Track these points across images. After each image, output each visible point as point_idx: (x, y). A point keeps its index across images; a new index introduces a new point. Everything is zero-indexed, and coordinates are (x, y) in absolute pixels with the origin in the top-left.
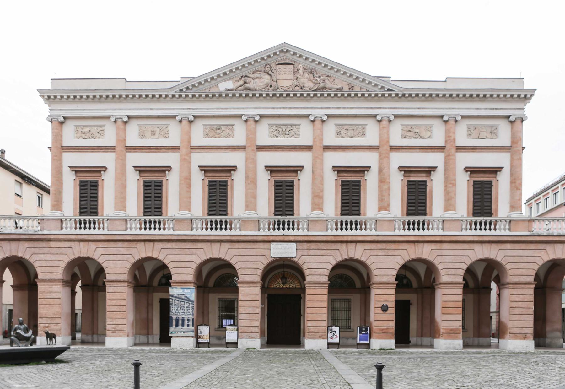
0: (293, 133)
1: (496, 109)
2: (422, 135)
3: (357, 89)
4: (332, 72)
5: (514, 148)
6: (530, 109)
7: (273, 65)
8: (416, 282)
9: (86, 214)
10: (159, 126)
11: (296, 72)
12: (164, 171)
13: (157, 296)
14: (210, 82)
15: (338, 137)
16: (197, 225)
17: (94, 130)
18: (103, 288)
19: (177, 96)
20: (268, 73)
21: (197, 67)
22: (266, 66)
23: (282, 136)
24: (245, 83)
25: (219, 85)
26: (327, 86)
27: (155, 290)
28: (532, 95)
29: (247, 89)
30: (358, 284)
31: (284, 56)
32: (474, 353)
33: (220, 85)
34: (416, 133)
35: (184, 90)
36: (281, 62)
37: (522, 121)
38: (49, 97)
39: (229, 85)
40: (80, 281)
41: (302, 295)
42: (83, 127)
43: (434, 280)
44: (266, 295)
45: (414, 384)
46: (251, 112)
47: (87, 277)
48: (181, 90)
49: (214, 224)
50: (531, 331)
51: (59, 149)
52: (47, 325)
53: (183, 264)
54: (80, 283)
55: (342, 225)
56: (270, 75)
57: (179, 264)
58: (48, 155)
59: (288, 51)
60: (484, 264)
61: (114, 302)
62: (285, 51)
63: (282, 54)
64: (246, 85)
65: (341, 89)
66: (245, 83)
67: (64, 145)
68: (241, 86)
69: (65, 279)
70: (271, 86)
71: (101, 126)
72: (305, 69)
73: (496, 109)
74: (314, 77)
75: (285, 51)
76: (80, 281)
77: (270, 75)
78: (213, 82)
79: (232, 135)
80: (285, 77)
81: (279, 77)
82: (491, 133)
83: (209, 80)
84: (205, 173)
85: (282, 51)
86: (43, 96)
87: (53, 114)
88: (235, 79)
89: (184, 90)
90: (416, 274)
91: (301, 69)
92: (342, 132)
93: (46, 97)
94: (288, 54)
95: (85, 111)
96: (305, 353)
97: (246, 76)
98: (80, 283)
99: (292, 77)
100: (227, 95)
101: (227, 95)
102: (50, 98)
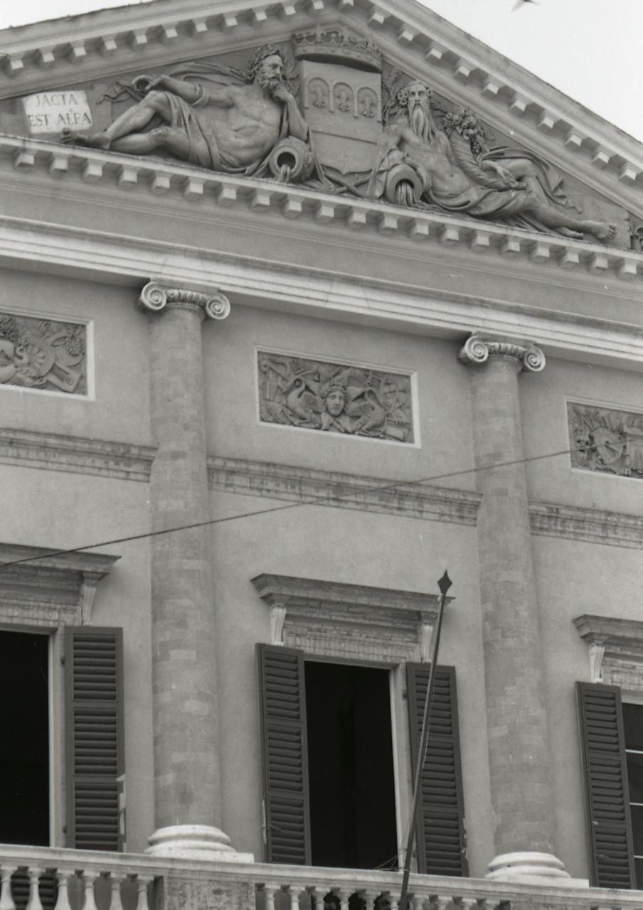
0: (378, 414)
12: (81, 577)
15: (586, 465)
23: (325, 419)
24: (159, 118)
29: (166, 151)
32: (515, 333)
33: (34, 106)
36: (325, 50)
46: (189, 272)
53: (439, 759)
56: (282, 104)
64: (162, 130)
68: (137, 130)
77: (282, 104)
79: (75, 376)
80: (340, 123)
81: (318, 121)
88: (101, 90)
92: (600, 440)
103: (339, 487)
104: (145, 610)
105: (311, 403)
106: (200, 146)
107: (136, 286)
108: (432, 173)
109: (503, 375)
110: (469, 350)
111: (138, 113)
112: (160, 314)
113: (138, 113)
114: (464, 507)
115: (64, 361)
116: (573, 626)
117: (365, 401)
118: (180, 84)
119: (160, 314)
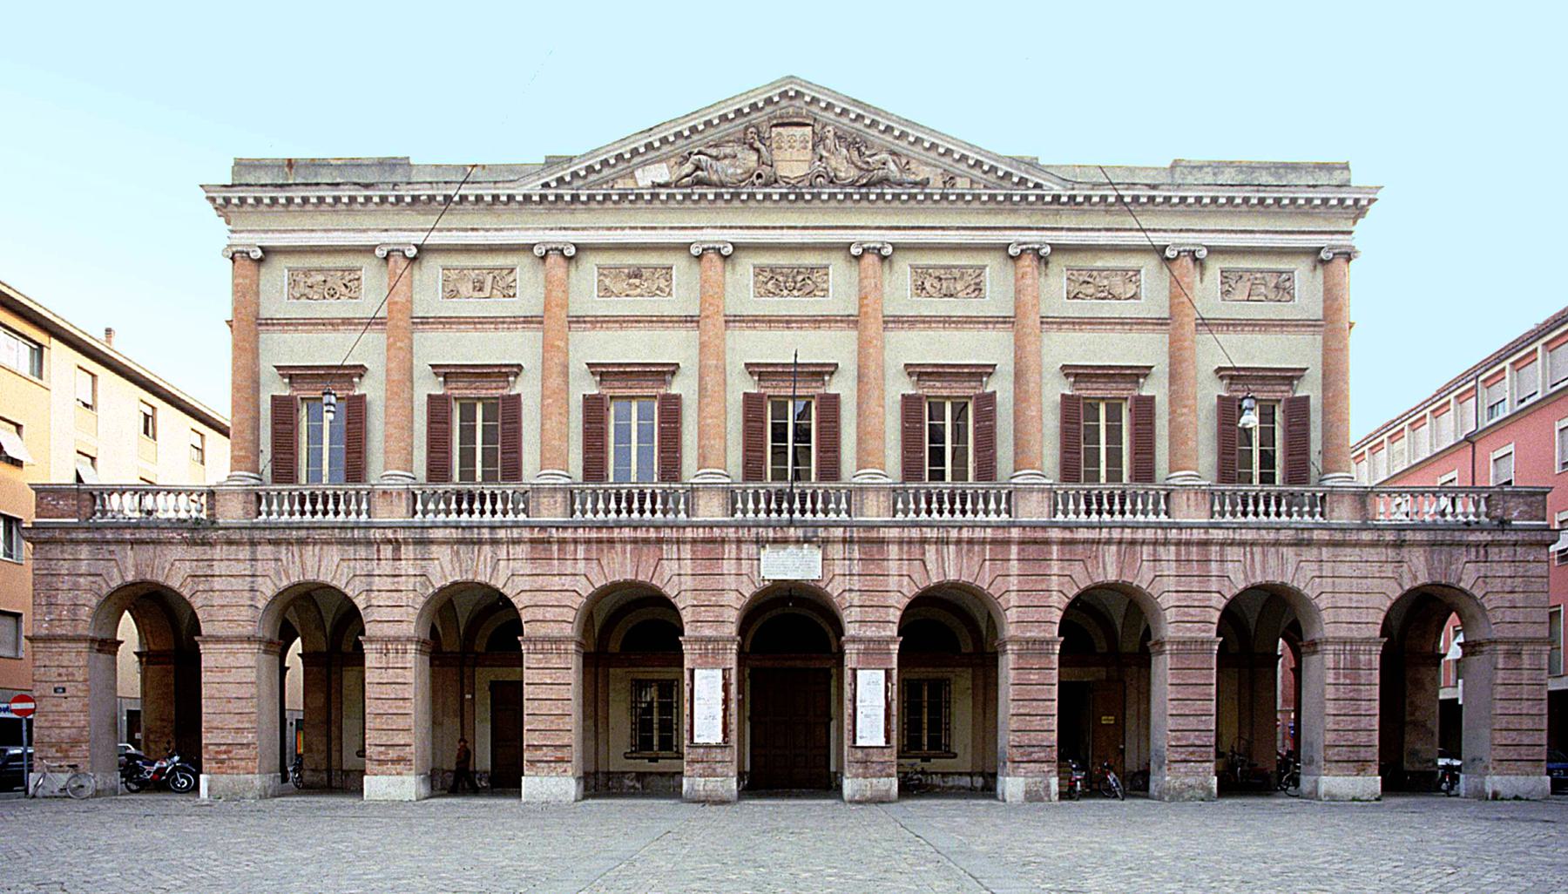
1: (942, 228)
2: (1116, 291)
3: (962, 184)
4: (904, 144)
5: (1330, 325)
6: (1363, 235)
7: (764, 128)
8: (790, 643)
9: (1232, 481)
10: (491, 270)
11: (818, 140)
13: (485, 676)
14: (614, 166)
16: (583, 504)
17: (336, 281)
18: (358, 658)
19: (536, 198)
20: (752, 147)
21: (587, 133)
22: (746, 128)
23: (785, 292)
24: (698, 168)
25: (638, 173)
26: (891, 176)
27: (481, 661)
28: (1371, 201)
30: (967, 647)
31: (788, 108)
34: (1100, 289)
35: (554, 184)
37: (1349, 260)
38: (227, 200)
39: (661, 173)
40: (299, 640)
41: (834, 671)
42: (307, 272)
43: (1147, 634)
44: (747, 671)
45: (1129, 877)
46: (872, 238)
47: (322, 630)
48: (546, 185)
49: (1117, 500)
50: (1374, 754)
51: (250, 325)
52: (223, 748)
54: (297, 646)
55: (642, 502)
56: (758, 150)
57: (541, 598)
58: (225, 338)
59: (799, 94)
60: (1265, 595)
61: (541, 693)
62: (792, 93)
63: (784, 103)
64: (699, 173)
65: (924, 183)
66: (698, 168)
67: (264, 314)
69: (268, 635)
70: (759, 176)
71: (351, 270)
72: (839, 138)
73: (942, 228)
74: (861, 154)
75: (792, 93)
76: (299, 640)
77: (758, 150)
78: (621, 166)
82: (1276, 287)
83: (612, 161)
84: (445, 382)
85: (784, 95)
86: (213, 200)
87: (236, 242)
88: (673, 161)
89: (554, 184)
90: (1104, 621)
91: (831, 135)
92: (927, 285)
93: (220, 201)
94: (797, 103)
95: (270, 235)
96: (364, 807)
97: (699, 153)
98: (297, 646)
99: (808, 154)
100: (655, 196)
101: (655, 196)
102: (225, 203)
103: (788, 322)
104: (853, 384)
105: (777, 286)
106: (715, 178)
107: (847, 247)
108: (835, 169)
109: (870, 259)
110: (1323, 255)
111: (688, 168)
112: (1329, 261)
113: (688, 168)
114: (851, 321)
115: (663, 283)
116: (1214, 376)
117: (804, 281)
118: (709, 151)
119: (1329, 261)
